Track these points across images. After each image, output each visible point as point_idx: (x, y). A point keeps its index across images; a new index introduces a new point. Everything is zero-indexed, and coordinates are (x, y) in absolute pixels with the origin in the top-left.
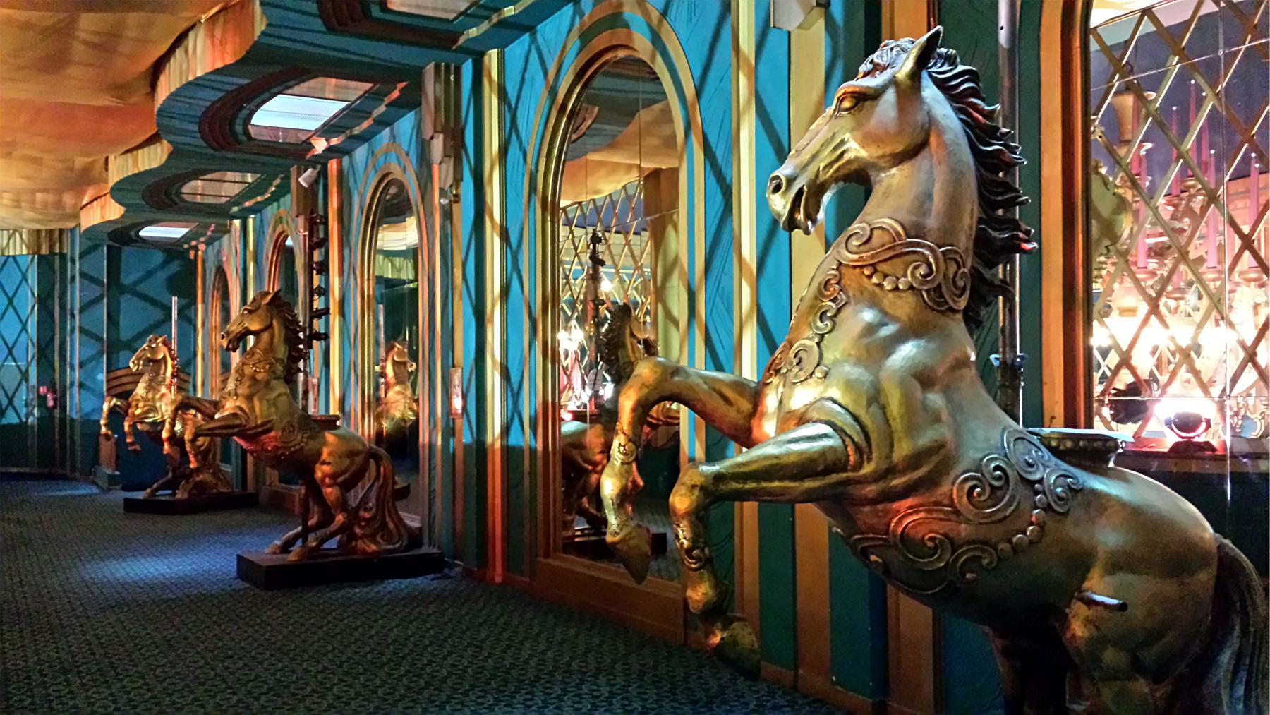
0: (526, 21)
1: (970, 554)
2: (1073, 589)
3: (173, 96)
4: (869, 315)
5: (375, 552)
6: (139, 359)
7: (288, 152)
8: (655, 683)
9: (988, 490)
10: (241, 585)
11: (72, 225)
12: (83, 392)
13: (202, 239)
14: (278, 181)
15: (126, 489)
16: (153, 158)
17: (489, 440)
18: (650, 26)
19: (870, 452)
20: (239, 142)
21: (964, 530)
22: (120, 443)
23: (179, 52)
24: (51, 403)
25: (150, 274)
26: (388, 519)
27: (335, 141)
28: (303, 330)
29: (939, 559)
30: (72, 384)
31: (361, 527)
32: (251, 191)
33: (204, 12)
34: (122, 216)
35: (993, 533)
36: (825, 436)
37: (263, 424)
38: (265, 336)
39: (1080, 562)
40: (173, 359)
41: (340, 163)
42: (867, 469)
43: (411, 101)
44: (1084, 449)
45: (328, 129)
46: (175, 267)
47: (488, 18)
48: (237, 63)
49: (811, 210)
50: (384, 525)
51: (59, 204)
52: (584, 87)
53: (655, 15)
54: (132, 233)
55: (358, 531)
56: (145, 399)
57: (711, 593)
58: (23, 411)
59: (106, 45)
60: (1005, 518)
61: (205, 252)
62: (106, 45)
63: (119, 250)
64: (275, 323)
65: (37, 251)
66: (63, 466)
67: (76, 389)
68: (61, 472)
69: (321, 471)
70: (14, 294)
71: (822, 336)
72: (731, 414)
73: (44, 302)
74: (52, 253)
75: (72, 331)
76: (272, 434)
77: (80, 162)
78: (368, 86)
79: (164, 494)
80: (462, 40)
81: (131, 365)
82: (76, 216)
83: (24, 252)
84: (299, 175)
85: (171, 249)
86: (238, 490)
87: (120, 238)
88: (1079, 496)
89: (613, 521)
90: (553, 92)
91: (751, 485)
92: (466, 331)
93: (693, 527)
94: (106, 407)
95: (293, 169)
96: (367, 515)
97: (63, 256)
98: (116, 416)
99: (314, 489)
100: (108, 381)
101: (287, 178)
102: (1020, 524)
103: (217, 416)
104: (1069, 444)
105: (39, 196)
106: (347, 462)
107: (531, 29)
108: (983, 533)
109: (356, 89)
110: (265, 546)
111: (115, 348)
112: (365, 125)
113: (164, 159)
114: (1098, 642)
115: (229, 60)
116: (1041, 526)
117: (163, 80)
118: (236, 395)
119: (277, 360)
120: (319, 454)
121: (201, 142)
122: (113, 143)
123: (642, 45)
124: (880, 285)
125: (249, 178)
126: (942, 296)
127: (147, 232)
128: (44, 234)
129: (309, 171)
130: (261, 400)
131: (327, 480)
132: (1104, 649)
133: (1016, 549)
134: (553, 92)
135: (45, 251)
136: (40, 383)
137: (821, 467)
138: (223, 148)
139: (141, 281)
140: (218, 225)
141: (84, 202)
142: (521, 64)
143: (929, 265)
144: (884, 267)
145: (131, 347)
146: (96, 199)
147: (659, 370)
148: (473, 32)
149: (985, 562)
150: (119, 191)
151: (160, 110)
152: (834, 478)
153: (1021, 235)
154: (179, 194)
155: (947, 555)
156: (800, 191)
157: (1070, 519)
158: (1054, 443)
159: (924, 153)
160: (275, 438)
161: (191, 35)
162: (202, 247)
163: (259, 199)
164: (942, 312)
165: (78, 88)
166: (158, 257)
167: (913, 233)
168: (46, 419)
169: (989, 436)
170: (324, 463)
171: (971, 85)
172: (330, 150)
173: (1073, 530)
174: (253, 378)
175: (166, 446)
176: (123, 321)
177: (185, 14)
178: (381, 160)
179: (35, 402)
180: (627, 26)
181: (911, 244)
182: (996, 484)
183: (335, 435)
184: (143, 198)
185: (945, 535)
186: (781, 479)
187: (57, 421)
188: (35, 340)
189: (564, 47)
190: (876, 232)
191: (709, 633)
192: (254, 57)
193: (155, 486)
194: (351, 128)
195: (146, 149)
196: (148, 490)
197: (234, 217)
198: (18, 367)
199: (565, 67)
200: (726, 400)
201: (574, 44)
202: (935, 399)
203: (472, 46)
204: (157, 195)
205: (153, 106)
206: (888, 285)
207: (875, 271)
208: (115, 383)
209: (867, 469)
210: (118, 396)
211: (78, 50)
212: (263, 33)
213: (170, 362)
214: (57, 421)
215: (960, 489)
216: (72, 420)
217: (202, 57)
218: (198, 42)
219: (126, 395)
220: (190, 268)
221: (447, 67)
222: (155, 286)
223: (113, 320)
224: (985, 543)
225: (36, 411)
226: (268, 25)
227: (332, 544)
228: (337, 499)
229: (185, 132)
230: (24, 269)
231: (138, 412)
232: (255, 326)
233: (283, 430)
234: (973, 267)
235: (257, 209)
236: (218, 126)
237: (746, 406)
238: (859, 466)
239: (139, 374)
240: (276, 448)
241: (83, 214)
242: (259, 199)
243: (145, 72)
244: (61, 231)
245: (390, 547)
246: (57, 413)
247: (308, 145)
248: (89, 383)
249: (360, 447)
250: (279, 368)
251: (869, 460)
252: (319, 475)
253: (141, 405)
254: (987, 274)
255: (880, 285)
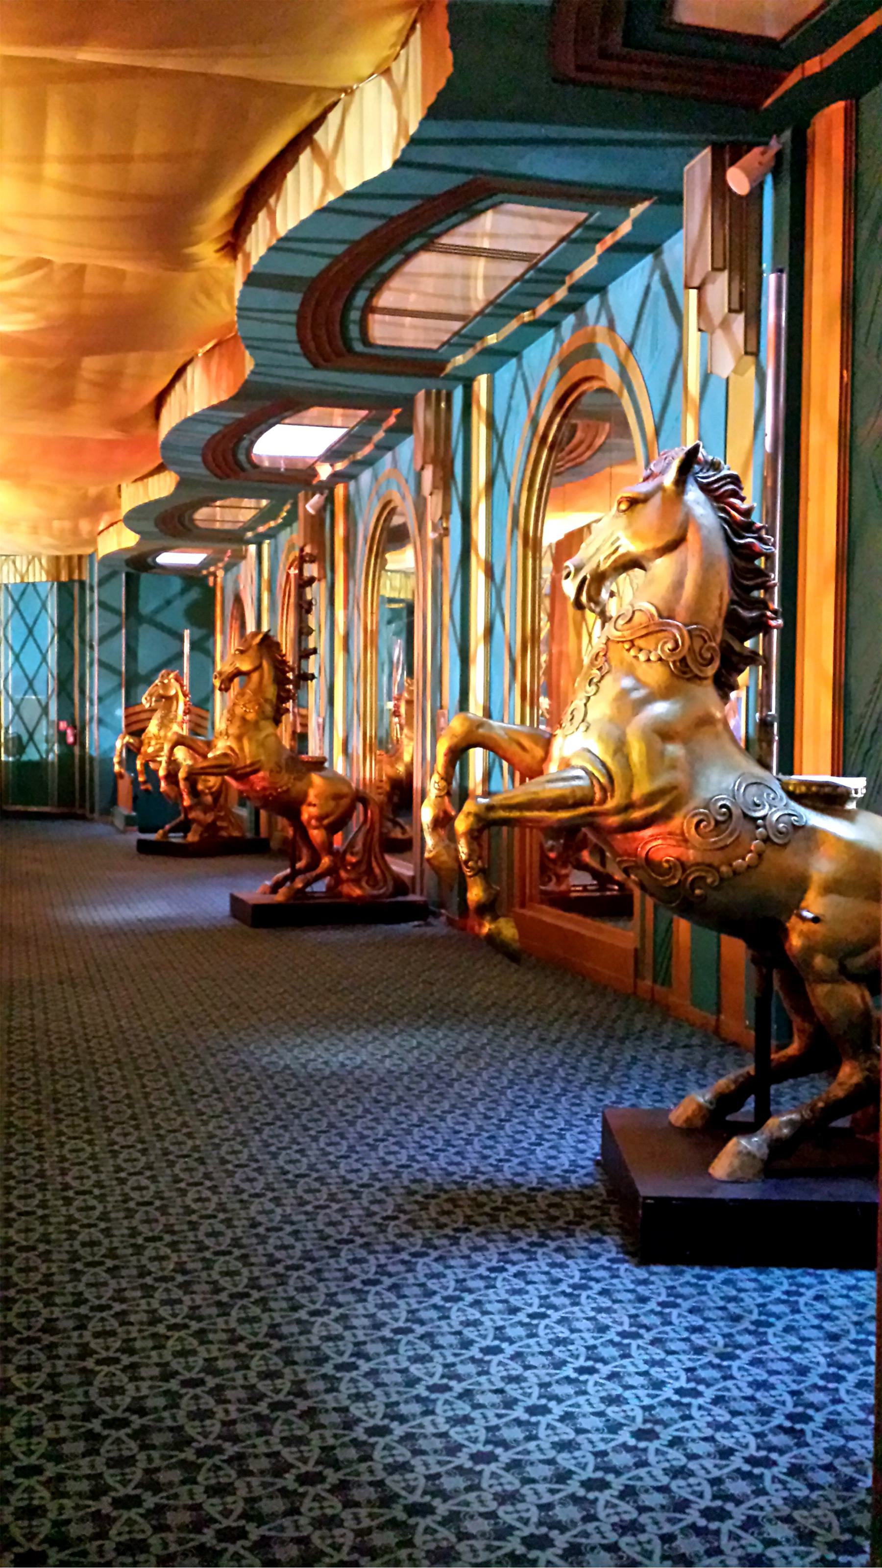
0: (509, 347)
1: (697, 874)
2: (794, 906)
3: (176, 430)
4: (627, 683)
5: (359, 898)
6: (151, 695)
7: (295, 479)
8: (581, 1022)
9: (713, 823)
10: (232, 921)
11: (89, 551)
12: (102, 729)
13: (220, 565)
14: (288, 507)
15: (142, 830)
16: (162, 486)
17: (471, 785)
18: (618, 356)
19: (613, 791)
20: (243, 469)
21: (691, 855)
22: (135, 782)
23: (178, 386)
24: (71, 739)
25: (168, 602)
26: (374, 864)
27: (340, 466)
28: (292, 670)
29: (674, 877)
30: (91, 719)
31: (347, 871)
32: (264, 516)
33: (201, 346)
34: (138, 544)
35: (716, 858)
36: (578, 778)
37: (252, 764)
38: (255, 676)
39: (799, 885)
40: (185, 695)
41: (346, 488)
42: (610, 804)
43: (405, 428)
44: (817, 794)
45: (332, 455)
46: (194, 594)
47: (472, 346)
48: (234, 398)
49: (593, 593)
50: (370, 871)
51: (75, 531)
52: (565, 416)
53: (623, 348)
54: (150, 560)
55: (343, 874)
56: (157, 737)
57: (481, 894)
58: (43, 747)
59: (109, 383)
60: (727, 846)
61: (224, 579)
62: (109, 383)
63: (138, 578)
64: (265, 664)
65: (57, 578)
66: (82, 806)
67: (95, 725)
68: (79, 812)
69: (307, 813)
70: (35, 623)
71: (588, 698)
72: (527, 759)
73: (64, 631)
74: (71, 580)
75: (91, 664)
76: (261, 774)
77: (93, 491)
78: (363, 413)
79: (176, 838)
80: (449, 368)
81: (144, 701)
82: (92, 541)
83: (44, 578)
84: (307, 500)
85: (191, 577)
86: (249, 835)
87: (138, 565)
88: (801, 833)
89: (430, 841)
90: (534, 422)
91: (515, 814)
92: (451, 671)
93: (469, 845)
94: (119, 744)
95: (301, 495)
96: (354, 860)
97: (82, 583)
98: (132, 752)
99: (301, 829)
100: (127, 717)
101: (295, 505)
102: (740, 851)
103: (210, 755)
104: (803, 789)
105: (56, 524)
106: (332, 804)
107: (517, 354)
108: (709, 858)
109: (355, 416)
110: (257, 886)
111: (134, 682)
112: (368, 449)
113: (172, 489)
114: (810, 950)
115: (224, 397)
116: (760, 855)
117: (165, 413)
118: (227, 734)
119: (266, 700)
120: (306, 795)
121: (203, 471)
122: (124, 472)
123: (612, 379)
124: (636, 657)
125: (264, 502)
126: (687, 666)
127: (164, 559)
128: (63, 560)
129: (317, 496)
130: (250, 740)
131: (313, 822)
132: (812, 957)
133: (735, 873)
134: (534, 422)
135: (64, 578)
136: (60, 718)
137: (570, 802)
138: (228, 476)
139: (157, 611)
140: (233, 551)
141: (101, 528)
142: (508, 388)
143: (676, 641)
144: (640, 643)
145: (148, 680)
146: (112, 525)
147: (467, 724)
148: (459, 360)
149: (709, 880)
150: (133, 519)
151: (163, 443)
152: (582, 810)
153: (769, 613)
154: (192, 520)
155: (679, 874)
156: (585, 579)
157: (789, 849)
158: (791, 788)
159: (682, 548)
160: (263, 779)
161: (189, 369)
162: (220, 573)
163: (272, 524)
164: (688, 680)
165: (85, 424)
166: (177, 584)
167: (665, 614)
168: (66, 758)
169: (725, 780)
170: (310, 805)
171: (731, 487)
172: (336, 477)
173: (789, 859)
174: (243, 719)
175: (163, 784)
176: (142, 653)
177: (181, 351)
178: (384, 487)
179: (55, 738)
180: (599, 357)
181: (662, 624)
182: (720, 818)
183: (322, 777)
184: (157, 525)
185: (678, 859)
186: (539, 810)
187: (77, 760)
188: (55, 672)
189: (545, 376)
190: (637, 614)
191: (481, 925)
192: (246, 393)
193: (167, 827)
194: (353, 453)
195: (156, 477)
196: (161, 832)
197: (249, 542)
198: (39, 701)
199: (546, 396)
200: (523, 748)
201: (554, 373)
202: (674, 749)
203: (461, 374)
204: (169, 522)
205: (157, 438)
206: (642, 657)
207: (633, 645)
208: (134, 718)
209: (610, 804)
210: (132, 734)
211: (83, 390)
212: (253, 373)
213: (181, 698)
214: (77, 760)
215: (689, 823)
216: (92, 759)
217: (199, 394)
218: (195, 375)
219: (138, 733)
220: (210, 594)
221: (438, 393)
222: (174, 616)
223: (132, 653)
224: (710, 865)
225: (56, 747)
226: (257, 365)
227: (320, 887)
228: (323, 843)
229: (189, 464)
230: (43, 596)
231: (150, 750)
232: (245, 667)
233: (271, 771)
234: (723, 641)
235: (271, 535)
236: (222, 456)
237: (539, 752)
238: (604, 801)
239: (153, 710)
240: (264, 789)
241: (100, 539)
242: (272, 524)
243: (150, 405)
244: (80, 557)
245: (375, 892)
246: (77, 750)
247: (311, 472)
248: (108, 719)
249: (345, 790)
250: (268, 709)
251: (612, 796)
252: (305, 816)
253: (153, 742)
254: (736, 646)
255: (636, 657)
